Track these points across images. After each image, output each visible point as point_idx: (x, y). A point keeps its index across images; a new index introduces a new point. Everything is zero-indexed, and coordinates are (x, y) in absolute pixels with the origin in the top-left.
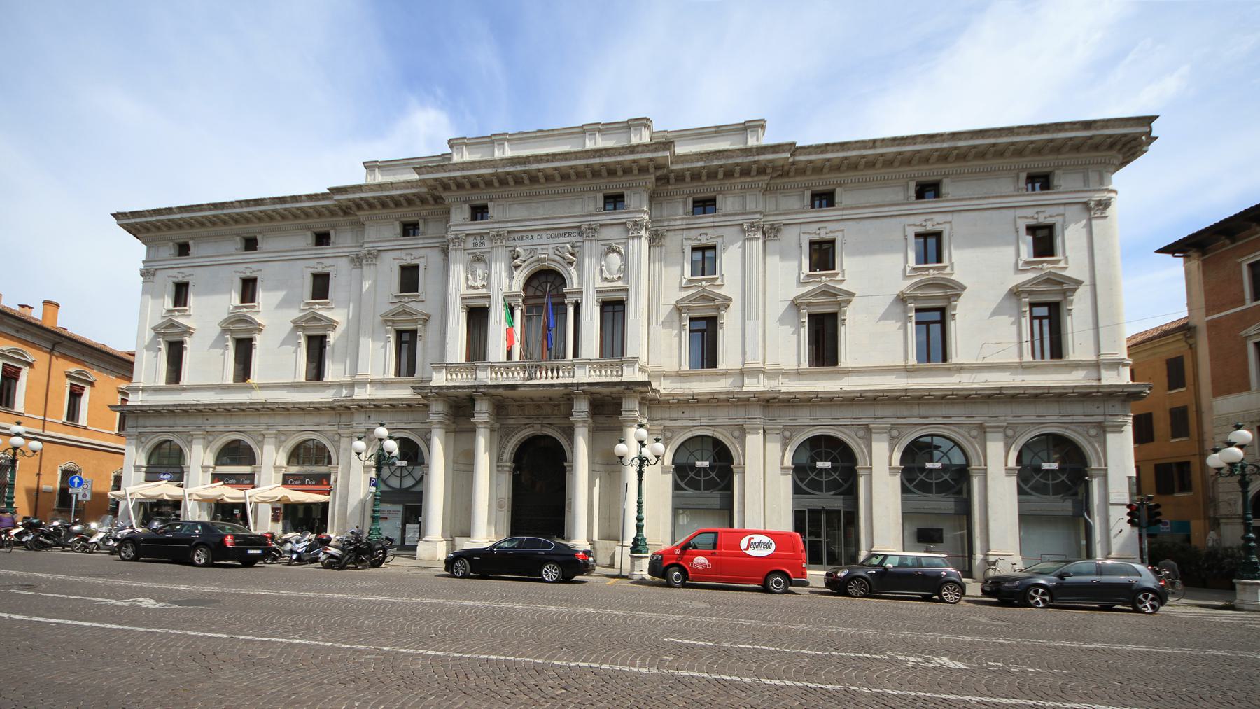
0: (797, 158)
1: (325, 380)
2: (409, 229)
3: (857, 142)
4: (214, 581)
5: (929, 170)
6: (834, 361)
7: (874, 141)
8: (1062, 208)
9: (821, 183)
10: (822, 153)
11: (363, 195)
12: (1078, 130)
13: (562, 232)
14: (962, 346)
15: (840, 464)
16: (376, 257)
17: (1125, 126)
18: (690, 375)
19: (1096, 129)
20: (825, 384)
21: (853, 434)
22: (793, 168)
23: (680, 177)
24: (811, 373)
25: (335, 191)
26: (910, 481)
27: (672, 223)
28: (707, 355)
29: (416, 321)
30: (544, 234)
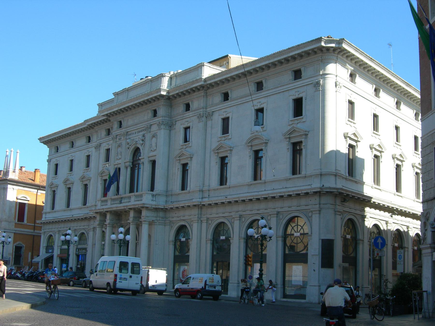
8: (305, 87)
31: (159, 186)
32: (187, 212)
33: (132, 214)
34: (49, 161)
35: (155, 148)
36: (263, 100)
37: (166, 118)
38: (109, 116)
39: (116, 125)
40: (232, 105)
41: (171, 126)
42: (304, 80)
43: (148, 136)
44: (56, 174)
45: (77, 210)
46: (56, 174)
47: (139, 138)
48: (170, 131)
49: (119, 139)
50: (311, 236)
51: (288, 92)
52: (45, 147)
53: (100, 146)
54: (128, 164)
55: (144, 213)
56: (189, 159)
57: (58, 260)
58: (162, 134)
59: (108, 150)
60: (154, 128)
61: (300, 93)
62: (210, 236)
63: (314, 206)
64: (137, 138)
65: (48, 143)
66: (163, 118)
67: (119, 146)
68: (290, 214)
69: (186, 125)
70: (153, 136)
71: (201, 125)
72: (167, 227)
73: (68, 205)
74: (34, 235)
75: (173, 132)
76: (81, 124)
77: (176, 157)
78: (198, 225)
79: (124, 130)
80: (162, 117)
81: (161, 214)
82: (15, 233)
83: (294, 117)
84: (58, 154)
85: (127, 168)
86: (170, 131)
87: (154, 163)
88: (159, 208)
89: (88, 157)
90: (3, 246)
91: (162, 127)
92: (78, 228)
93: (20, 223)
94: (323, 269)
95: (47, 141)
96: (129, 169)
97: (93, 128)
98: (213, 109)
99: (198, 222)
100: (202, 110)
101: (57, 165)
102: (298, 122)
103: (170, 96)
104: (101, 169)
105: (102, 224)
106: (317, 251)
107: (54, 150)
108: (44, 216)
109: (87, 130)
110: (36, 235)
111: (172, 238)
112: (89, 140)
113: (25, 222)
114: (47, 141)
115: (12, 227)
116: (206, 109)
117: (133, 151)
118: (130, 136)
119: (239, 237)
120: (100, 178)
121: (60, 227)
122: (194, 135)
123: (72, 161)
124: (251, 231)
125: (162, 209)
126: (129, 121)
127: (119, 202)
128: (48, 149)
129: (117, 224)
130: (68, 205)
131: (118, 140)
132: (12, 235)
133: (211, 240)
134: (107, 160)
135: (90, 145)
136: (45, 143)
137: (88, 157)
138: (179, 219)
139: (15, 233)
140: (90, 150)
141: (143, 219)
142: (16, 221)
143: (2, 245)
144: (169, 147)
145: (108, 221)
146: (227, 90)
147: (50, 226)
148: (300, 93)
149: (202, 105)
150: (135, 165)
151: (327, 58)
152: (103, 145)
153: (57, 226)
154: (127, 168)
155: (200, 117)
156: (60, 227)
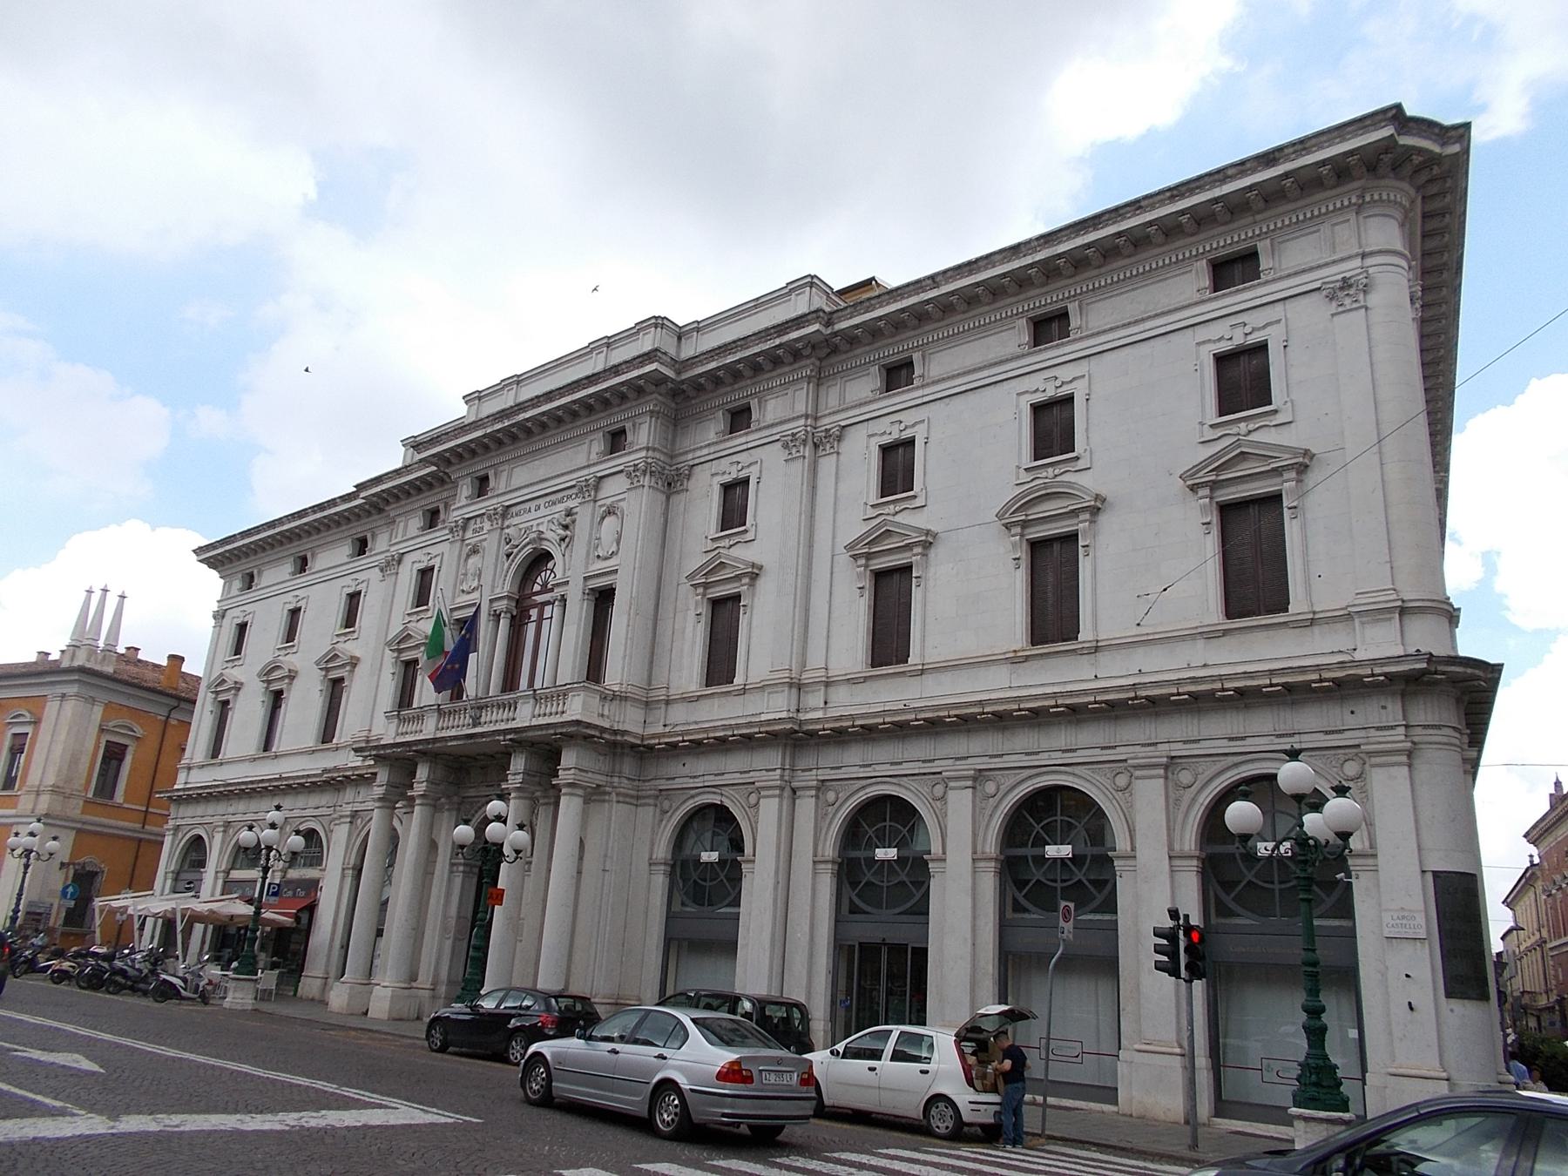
0: (838, 327)
1: (1081, 637)
2: (1232, 270)
3: (908, 285)
4: (1141, 1117)
5: (1042, 287)
6: (1071, 632)
7: (932, 277)
8: (1279, 307)
9: (892, 352)
10: (971, 273)
11: (384, 487)
12: (1254, 171)
13: (560, 495)
14: (1104, 602)
15: (1029, 851)
16: (839, 439)
17: (1343, 140)
18: (1226, 632)
19: (1288, 159)
20: (1263, 652)
21: (925, 790)
22: (1387, 158)
23: (697, 386)
24: (1226, 632)
25: (361, 487)
26: (1227, 886)
27: (698, 453)
28: (889, 641)
29: (1277, 472)
30: (541, 501)
31: (616, 672)
32: (733, 766)
33: (518, 764)
34: (219, 616)
35: (614, 548)
36: (1065, 373)
37: (657, 455)
38: (449, 463)
39: (465, 490)
40: (926, 399)
41: (671, 480)
42: (1267, 282)
43: (584, 517)
44: (238, 651)
45: (297, 753)
46: (238, 650)
47: (551, 521)
48: (668, 498)
49: (475, 531)
50: (1374, 856)
51: (1189, 331)
52: (214, 574)
53: (399, 562)
54: (502, 605)
55: (569, 758)
56: (746, 580)
57: (458, 881)
58: (638, 505)
59: (426, 574)
60: (614, 488)
61: (1254, 330)
62: (829, 850)
63: (1373, 732)
64: (540, 522)
65: (223, 564)
66: (650, 453)
67: (475, 551)
68: (1236, 765)
69: (733, 474)
70: (610, 512)
71: (799, 468)
72: (647, 814)
73: (267, 744)
74: (140, 840)
75: (675, 499)
76: (346, 498)
77: (690, 577)
78: (781, 805)
79: (495, 501)
80: (648, 449)
81: (628, 766)
82: (79, 831)
83: (1221, 415)
84: (251, 596)
85: (497, 617)
86: (668, 498)
87: (603, 599)
88: (623, 745)
89: (354, 598)
90: (27, 866)
91: (646, 481)
92: (296, 813)
93: (99, 800)
94: (1456, 1004)
95: (219, 557)
96: (504, 624)
97: (381, 511)
98: (842, 419)
99: (780, 796)
100: (802, 422)
101: (242, 628)
102: (1251, 427)
103: (683, 382)
104: (396, 629)
105: (398, 794)
106: (1420, 919)
107: (237, 584)
108: (182, 777)
109: (359, 517)
110: (149, 841)
111: (663, 850)
112: (362, 547)
113: (119, 797)
114: (219, 557)
115: (75, 809)
116: (816, 419)
117: (522, 571)
118: (515, 520)
119: (974, 852)
120: (389, 656)
121: (231, 810)
122: (770, 508)
123: (295, 612)
124: (1241, 813)
125: (633, 746)
126: (516, 478)
127: (468, 720)
128: (222, 581)
129: (448, 797)
130: (267, 744)
131: (469, 534)
132: (68, 838)
133: (833, 862)
134: (422, 597)
135: (364, 561)
136: (212, 563)
137: (354, 598)
138: (701, 779)
139: (79, 831)
140: (361, 576)
141: (564, 777)
142: (90, 795)
143: (24, 860)
144: (663, 546)
145: (419, 788)
146: (906, 355)
147: (199, 809)
148: (1254, 330)
149: (801, 408)
150: (520, 612)
151: (1376, 197)
152: (408, 559)
153: (221, 808)
154: (497, 617)
155: (790, 442)
156: (231, 810)
